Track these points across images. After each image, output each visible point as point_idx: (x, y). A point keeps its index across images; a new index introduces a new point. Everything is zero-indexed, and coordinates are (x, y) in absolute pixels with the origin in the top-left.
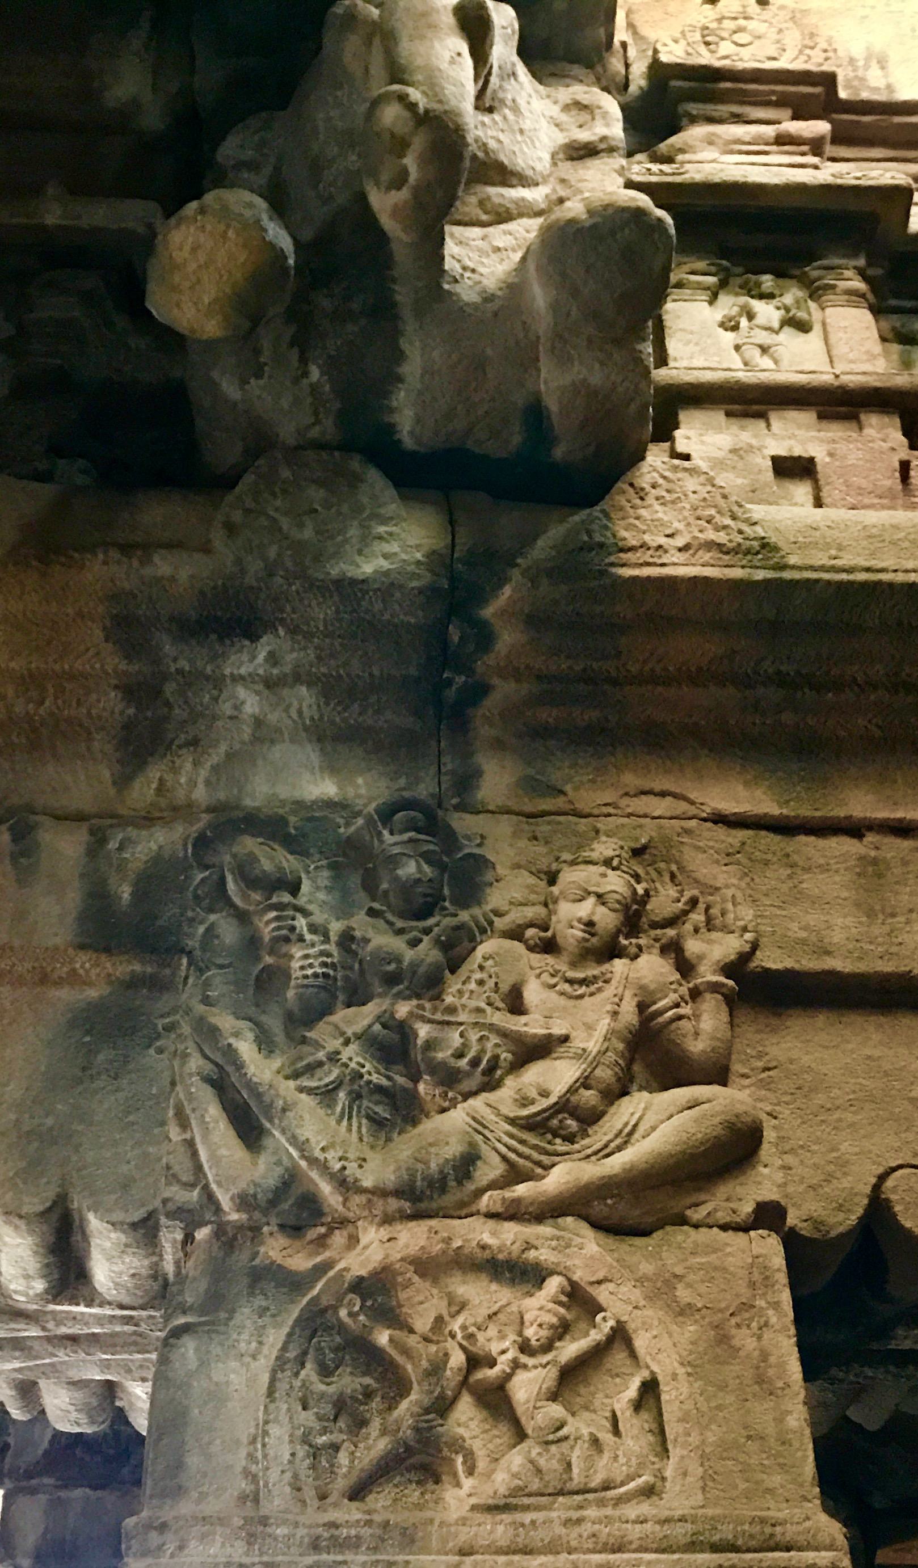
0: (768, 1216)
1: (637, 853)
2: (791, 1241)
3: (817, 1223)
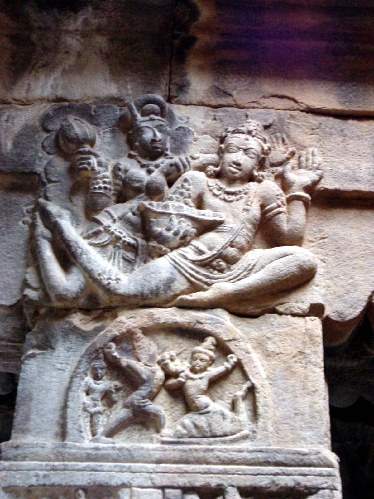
0: (316, 310)
1: (266, 127)
2: (327, 323)
3: (340, 314)
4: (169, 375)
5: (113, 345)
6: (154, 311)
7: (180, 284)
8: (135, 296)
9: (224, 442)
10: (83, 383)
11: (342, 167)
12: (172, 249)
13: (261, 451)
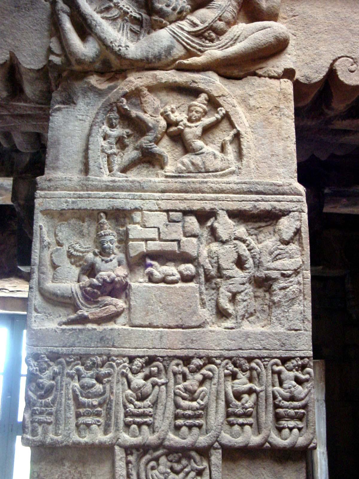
0: (289, 74)
2: (297, 85)
3: (307, 78)
6: (157, 73)
9: (216, 176)
10: (100, 130)
12: (171, 23)
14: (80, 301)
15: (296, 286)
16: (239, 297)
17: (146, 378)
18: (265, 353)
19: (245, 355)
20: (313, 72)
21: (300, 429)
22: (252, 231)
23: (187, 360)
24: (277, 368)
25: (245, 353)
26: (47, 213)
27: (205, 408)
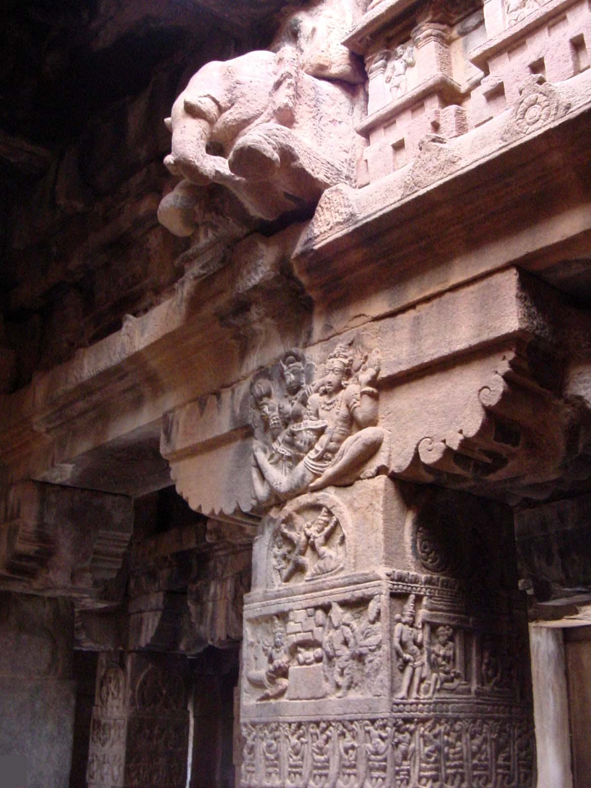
0: (381, 470)
1: (350, 345)
2: (393, 477)
3: (399, 467)
4: (308, 537)
5: (283, 525)
6: (299, 498)
7: (309, 477)
8: (289, 491)
9: (331, 575)
10: (272, 553)
11: (391, 356)
12: (306, 453)
13: (347, 577)
14: (266, 683)
15: (378, 658)
16: (345, 672)
17: (298, 738)
18: (359, 716)
19: (348, 719)
20: (400, 463)
21: (384, 779)
22: (356, 615)
23: (317, 724)
24: (367, 728)
25: (347, 717)
26: (249, 620)
27: (328, 761)
